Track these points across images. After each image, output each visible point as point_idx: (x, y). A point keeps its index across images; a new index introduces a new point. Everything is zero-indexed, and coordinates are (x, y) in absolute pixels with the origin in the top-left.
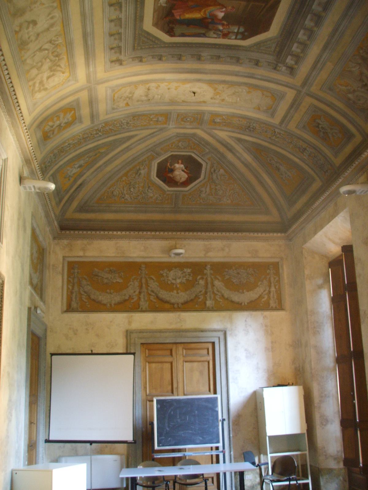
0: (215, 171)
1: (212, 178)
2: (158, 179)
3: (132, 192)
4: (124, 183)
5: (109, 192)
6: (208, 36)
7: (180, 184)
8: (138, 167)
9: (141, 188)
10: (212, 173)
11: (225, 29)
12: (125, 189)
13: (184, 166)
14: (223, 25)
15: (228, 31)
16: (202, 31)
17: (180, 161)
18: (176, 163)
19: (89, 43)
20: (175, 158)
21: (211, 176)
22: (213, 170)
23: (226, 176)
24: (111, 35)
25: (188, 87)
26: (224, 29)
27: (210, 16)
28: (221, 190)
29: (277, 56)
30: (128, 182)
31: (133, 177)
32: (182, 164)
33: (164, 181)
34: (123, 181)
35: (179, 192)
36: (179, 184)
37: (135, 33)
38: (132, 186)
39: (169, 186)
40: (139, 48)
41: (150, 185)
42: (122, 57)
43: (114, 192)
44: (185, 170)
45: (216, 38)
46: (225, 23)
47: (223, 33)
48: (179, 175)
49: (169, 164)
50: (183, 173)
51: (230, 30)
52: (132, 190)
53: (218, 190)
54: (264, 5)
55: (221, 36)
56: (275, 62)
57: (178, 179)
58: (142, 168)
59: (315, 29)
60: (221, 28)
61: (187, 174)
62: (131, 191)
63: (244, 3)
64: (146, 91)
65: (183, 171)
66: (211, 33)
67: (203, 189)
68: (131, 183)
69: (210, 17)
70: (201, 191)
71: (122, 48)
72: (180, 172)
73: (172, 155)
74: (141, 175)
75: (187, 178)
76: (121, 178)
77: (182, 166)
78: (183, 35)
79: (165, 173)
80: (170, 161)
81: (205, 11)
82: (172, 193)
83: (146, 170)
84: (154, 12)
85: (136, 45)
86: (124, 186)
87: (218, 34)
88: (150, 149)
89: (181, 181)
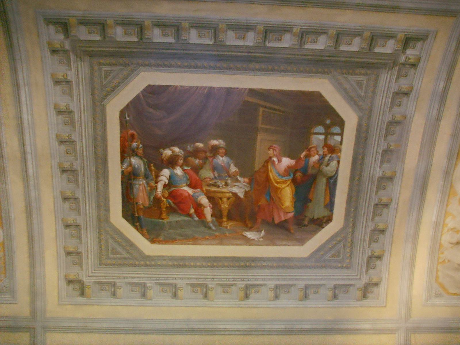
11: (318, 152)
14: (308, 156)
15: (323, 147)
16: (322, 183)
24: (66, 199)
27: (290, 175)
40: (348, 261)
42: (361, 284)
45: (339, 162)
46: (304, 153)
51: (322, 144)
54: (261, 109)
55: (334, 155)
59: (296, 30)
63: (260, 136)
78: (330, 206)
81: (277, 183)
84: (275, 245)
85: (339, 265)
87: (329, 160)
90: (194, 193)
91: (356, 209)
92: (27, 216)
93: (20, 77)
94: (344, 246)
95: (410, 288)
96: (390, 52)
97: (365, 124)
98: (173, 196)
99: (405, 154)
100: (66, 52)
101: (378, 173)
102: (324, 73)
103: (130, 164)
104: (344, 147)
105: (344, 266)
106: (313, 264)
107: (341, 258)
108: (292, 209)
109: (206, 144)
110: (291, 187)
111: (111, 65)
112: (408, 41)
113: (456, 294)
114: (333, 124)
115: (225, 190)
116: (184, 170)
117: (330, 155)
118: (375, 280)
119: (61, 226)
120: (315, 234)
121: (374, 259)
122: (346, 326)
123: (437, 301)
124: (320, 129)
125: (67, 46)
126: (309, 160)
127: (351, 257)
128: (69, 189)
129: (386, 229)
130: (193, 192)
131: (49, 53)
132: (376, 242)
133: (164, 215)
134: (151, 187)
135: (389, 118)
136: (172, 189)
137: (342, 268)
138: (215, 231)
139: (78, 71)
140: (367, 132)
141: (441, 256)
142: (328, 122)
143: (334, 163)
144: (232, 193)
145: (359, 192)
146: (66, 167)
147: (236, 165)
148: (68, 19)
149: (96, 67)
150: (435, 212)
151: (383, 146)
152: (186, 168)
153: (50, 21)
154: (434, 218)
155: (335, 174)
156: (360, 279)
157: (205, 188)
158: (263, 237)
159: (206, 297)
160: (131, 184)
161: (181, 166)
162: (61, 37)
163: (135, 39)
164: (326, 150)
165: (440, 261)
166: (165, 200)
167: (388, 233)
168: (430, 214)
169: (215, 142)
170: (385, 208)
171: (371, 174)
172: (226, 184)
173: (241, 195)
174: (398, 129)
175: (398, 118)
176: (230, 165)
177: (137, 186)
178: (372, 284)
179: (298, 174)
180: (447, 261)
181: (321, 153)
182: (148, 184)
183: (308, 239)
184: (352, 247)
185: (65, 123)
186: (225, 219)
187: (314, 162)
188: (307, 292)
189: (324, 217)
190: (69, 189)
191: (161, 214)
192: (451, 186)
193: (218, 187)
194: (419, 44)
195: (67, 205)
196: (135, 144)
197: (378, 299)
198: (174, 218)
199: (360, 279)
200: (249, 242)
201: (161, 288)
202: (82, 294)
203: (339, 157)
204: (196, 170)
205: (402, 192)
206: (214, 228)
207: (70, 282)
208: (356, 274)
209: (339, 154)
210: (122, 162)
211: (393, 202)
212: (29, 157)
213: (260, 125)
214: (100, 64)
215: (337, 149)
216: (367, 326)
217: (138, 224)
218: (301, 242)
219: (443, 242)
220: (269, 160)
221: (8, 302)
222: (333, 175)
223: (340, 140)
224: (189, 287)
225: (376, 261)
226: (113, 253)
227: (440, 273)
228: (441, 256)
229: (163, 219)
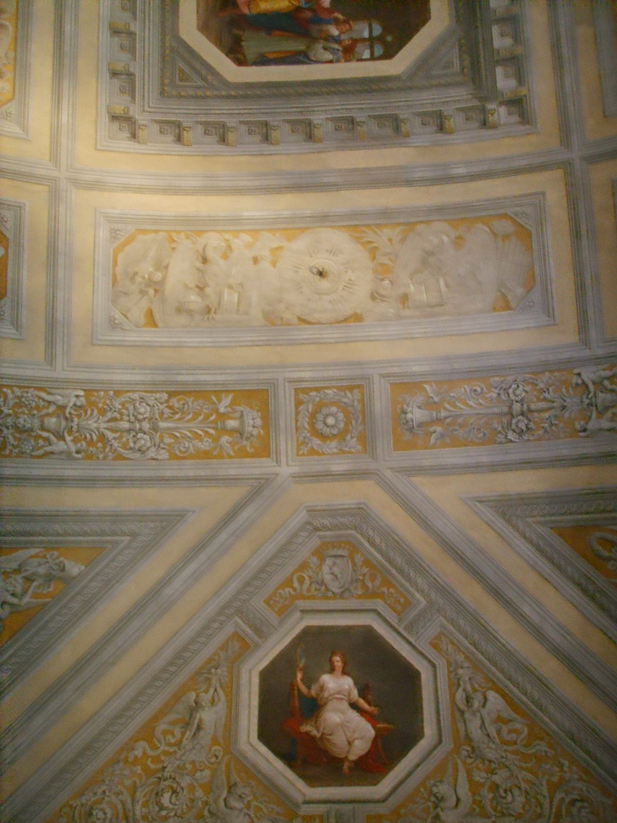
0: (468, 700)
1: (468, 738)
2: (263, 749)
3: (167, 808)
4: (139, 769)
5: (78, 808)
6: (313, 59)
7: (350, 769)
8: (193, 696)
9: (200, 793)
10: (462, 713)
11: (344, 33)
12: (139, 795)
13: (356, 683)
14: (337, 22)
15: (352, 39)
16: (298, 45)
17: (337, 660)
18: (325, 672)
19: (67, 28)
20: (317, 645)
21: (461, 726)
22: (460, 695)
23: (518, 726)
25: (302, 252)
26: (342, 33)
27: (306, 3)
28: (516, 792)
29: (474, 83)
30: (153, 766)
31: (173, 741)
32: (344, 672)
33: (288, 758)
34: (136, 761)
35: (350, 806)
36: (346, 766)
37: (163, 47)
38: (166, 783)
39: (312, 781)
41: (235, 777)
42: (135, 112)
43: (94, 812)
44: (362, 703)
45: (331, 62)
46: (340, 16)
47: (344, 44)
48: (342, 725)
49: (299, 676)
50: (354, 715)
51: (355, 36)
52: (166, 799)
53: (505, 791)
55: (340, 54)
56: (476, 103)
57: (338, 743)
58: (206, 698)
60: (334, 31)
61: (369, 721)
62: (162, 808)
64: (199, 265)
65: (354, 706)
66: (319, 51)
67: (444, 789)
68: (164, 768)
69: (307, 6)
70: (439, 800)
71: (137, 77)
72: (346, 724)
73: (307, 633)
74: (202, 733)
75: (375, 741)
76: (129, 747)
77: (347, 683)
78: (263, 61)
79: (288, 720)
80: (302, 664)
82: (322, 809)
83: (221, 706)
86: (138, 784)
87: (333, 49)
88: (227, 606)
89: (353, 757)
91: (260, 97)
94: (198, 87)
95: (126, 188)
96: (498, 87)
97: (390, 85)
99: (350, 148)
101: (318, 118)
102: (457, 17)
104: (353, 65)
105: (166, 88)
106: (167, 45)
107: (178, 83)
108: (254, 11)
110: (288, 7)
112: (517, 104)
113: (115, 263)
114: (386, 45)
117: (340, 49)
118: (141, 133)
120: (216, 45)
121: (177, 131)
122: (65, 92)
123: (103, 233)
124: (377, 30)
126: (331, 24)
127: (179, 96)
128: (122, 61)
129: (228, 144)
132: (205, 132)
135: (403, 115)
137: (163, 84)
140: (380, 90)
141: (182, 235)
142: (389, 39)
143: (329, 56)
145: (287, 96)
150: (257, 214)
151: (360, 117)
154: (246, 214)
155: (313, 61)
156: (144, 111)
164: (347, 43)
165: (174, 234)
167: (221, 148)
168: (252, 207)
170: (262, 137)
171: (316, 109)
174: (389, 131)
175: (404, 128)
178: (135, 129)
179: (308, 14)
180: (174, 245)
181: (343, 37)
183: (208, 37)
184: (196, 97)
187: (328, 31)
188: (123, 35)
189: (243, 54)
190: (122, 61)
192: (302, 230)
194: (515, 118)
197: (110, 138)
199: (144, 111)
203: (338, 61)
205: (291, 157)
208: (151, 105)
209: (343, 60)
211: (272, 148)
215: (350, 57)
216: (64, 118)
218: (204, 28)
219: (206, 235)
222: (311, 58)
223: (363, 57)
225: (173, 134)
227: (151, 236)
228: (182, 235)
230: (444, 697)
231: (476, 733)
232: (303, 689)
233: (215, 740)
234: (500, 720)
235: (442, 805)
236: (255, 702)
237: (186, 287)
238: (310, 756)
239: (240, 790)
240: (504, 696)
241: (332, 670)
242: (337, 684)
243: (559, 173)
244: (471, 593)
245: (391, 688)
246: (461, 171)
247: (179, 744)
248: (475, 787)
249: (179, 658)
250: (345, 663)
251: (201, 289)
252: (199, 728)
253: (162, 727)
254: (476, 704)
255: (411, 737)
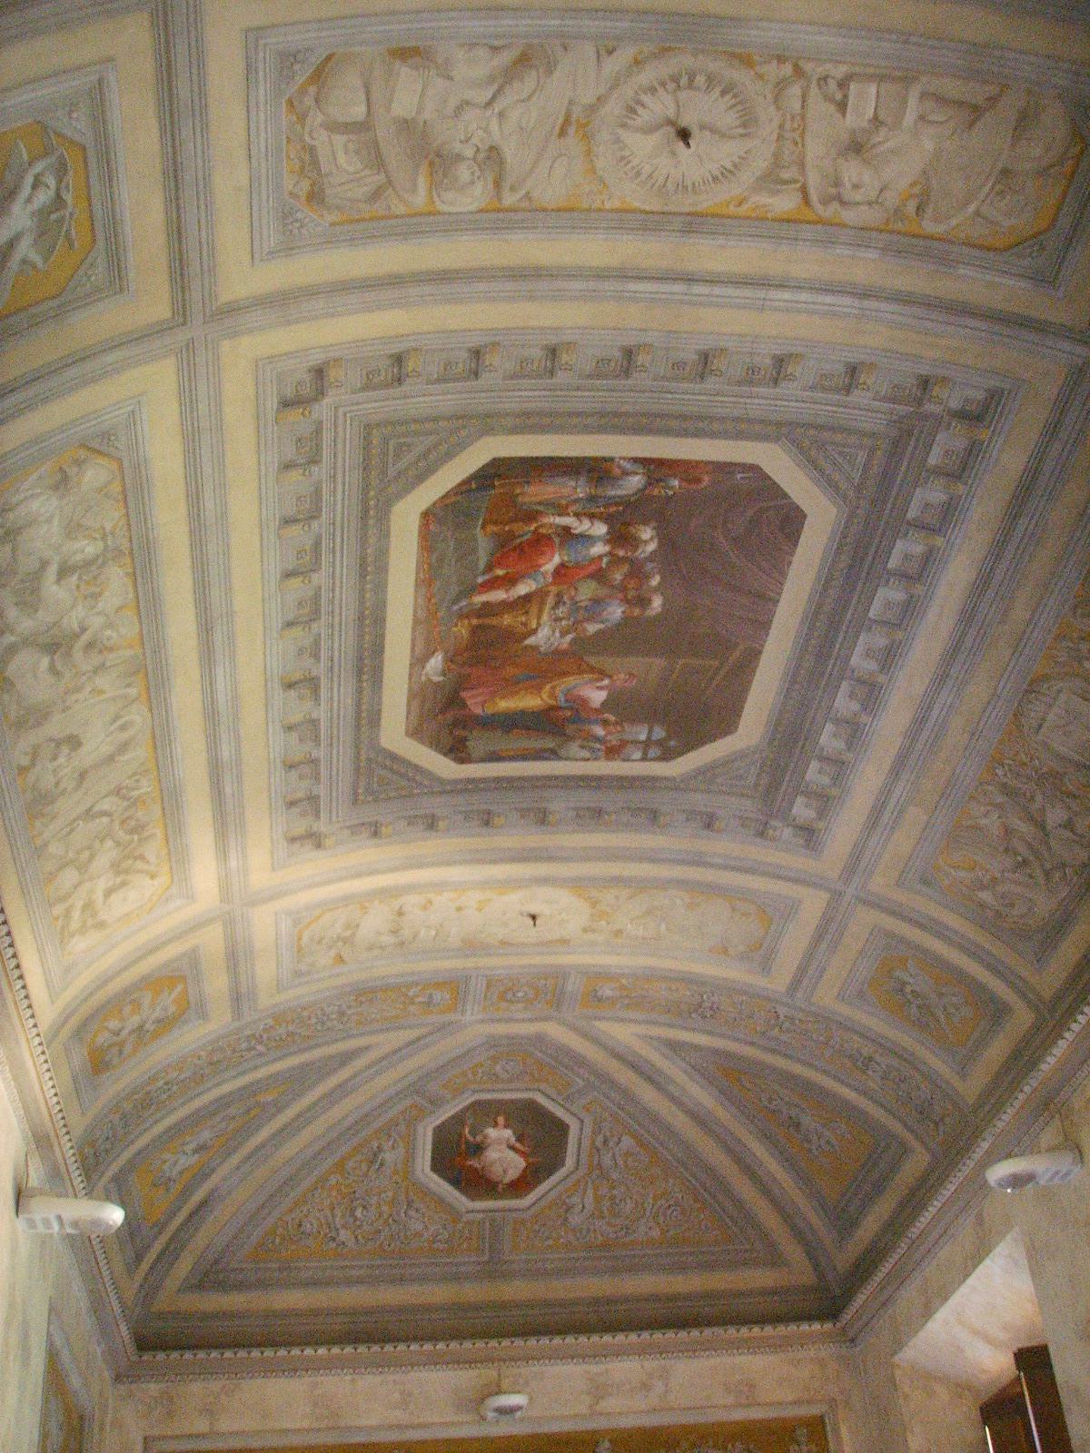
0: (605, 1142)
8: (376, 1144)
9: (385, 1208)
14: (605, 723)
16: (549, 743)
17: (501, 1120)
22: (600, 1139)
28: (629, 1201)
32: (506, 1126)
33: (455, 1182)
34: (331, 1189)
42: (321, 826)
44: (518, 1145)
46: (612, 718)
50: (512, 1154)
51: (625, 737)
52: (359, 1213)
57: (496, 1172)
59: (864, 719)
60: (599, 731)
65: (512, 1148)
66: (574, 749)
67: (575, 1200)
68: (354, 1192)
72: (502, 1153)
73: (478, 1103)
77: (508, 1133)
79: (457, 1159)
83: (401, 1150)
89: (507, 1180)
90: (544, 575)
92: (510, 269)
93: (884, 306)
98: (540, 542)
100: (920, 402)
102: (772, 740)
103: (626, 473)
109: (656, 590)
111: (866, 468)
115: (545, 617)
116: (600, 557)
119: (475, 341)
125: (930, 407)
130: (546, 573)
131: (925, 373)
133: (492, 528)
134: (567, 506)
136: (557, 540)
138: (449, 608)
139: (867, 410)
143: (586, 754)
144: (537, 629)
146: (640, 358)
147: (597, 634)
148: (989, 427)
149: (867, 442)
152: (605, 560)
153: (994, 396)
157: (554, 589)
158: (429, 680)
159: (286, 522)
160: (578, 473)
161: (610, 553)
162: (954, 404)
163: (911, 514)
166: (532, 528)
169: (657, 602)
172: (558, 619)
173: (531, 641)
176: (602, 622)
177: (573, 484)
182: (576, 501)
185: (752, 370)
186: (475, 621)
191: (496, 523)
193: (554, 608)
195: (537, 353)
196: (676, 483)
198: (484, 546)
200: (419, 661)
201: (307, 548)
202: (286, 404)
204: (599, 576)
206: (456, 608)
207: (319, 372)
210: (636, 460)
212: (678, 288)
213: (682, 661)
214: (873, 450)
217: (474, 486)
220: (603, 674)
221: (256, 243)
223: (633, 758)
224: (311, 593)
226: (401, 445)
229: (483, 527)
230: (586, 1143)
231: (607, 1160)
232: (470, 1138)
233: (396, 1172)
234: (628, 1154)
235: (572, 1210)
236: (429, 1147)
237: (379, 933)
238: (475, 1182)
239: (415, 1205)
240: (635, 1137)
241: (496, 1125)
242: (499, 1135)
243: (825, 896)
244: (625, 1076)
245: (543, 1137)
246: (718, 860)
247: (366, 1175)
248: (598, 1199)
249: (365, 1119)
250: (506, 1120)
251: (394, 932)
252: (381, 1165)
253: (351, 1164)
254: (611, 1144)
255: (557, 1163)
